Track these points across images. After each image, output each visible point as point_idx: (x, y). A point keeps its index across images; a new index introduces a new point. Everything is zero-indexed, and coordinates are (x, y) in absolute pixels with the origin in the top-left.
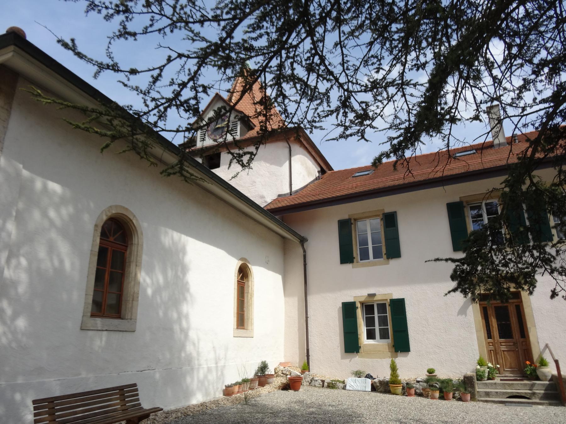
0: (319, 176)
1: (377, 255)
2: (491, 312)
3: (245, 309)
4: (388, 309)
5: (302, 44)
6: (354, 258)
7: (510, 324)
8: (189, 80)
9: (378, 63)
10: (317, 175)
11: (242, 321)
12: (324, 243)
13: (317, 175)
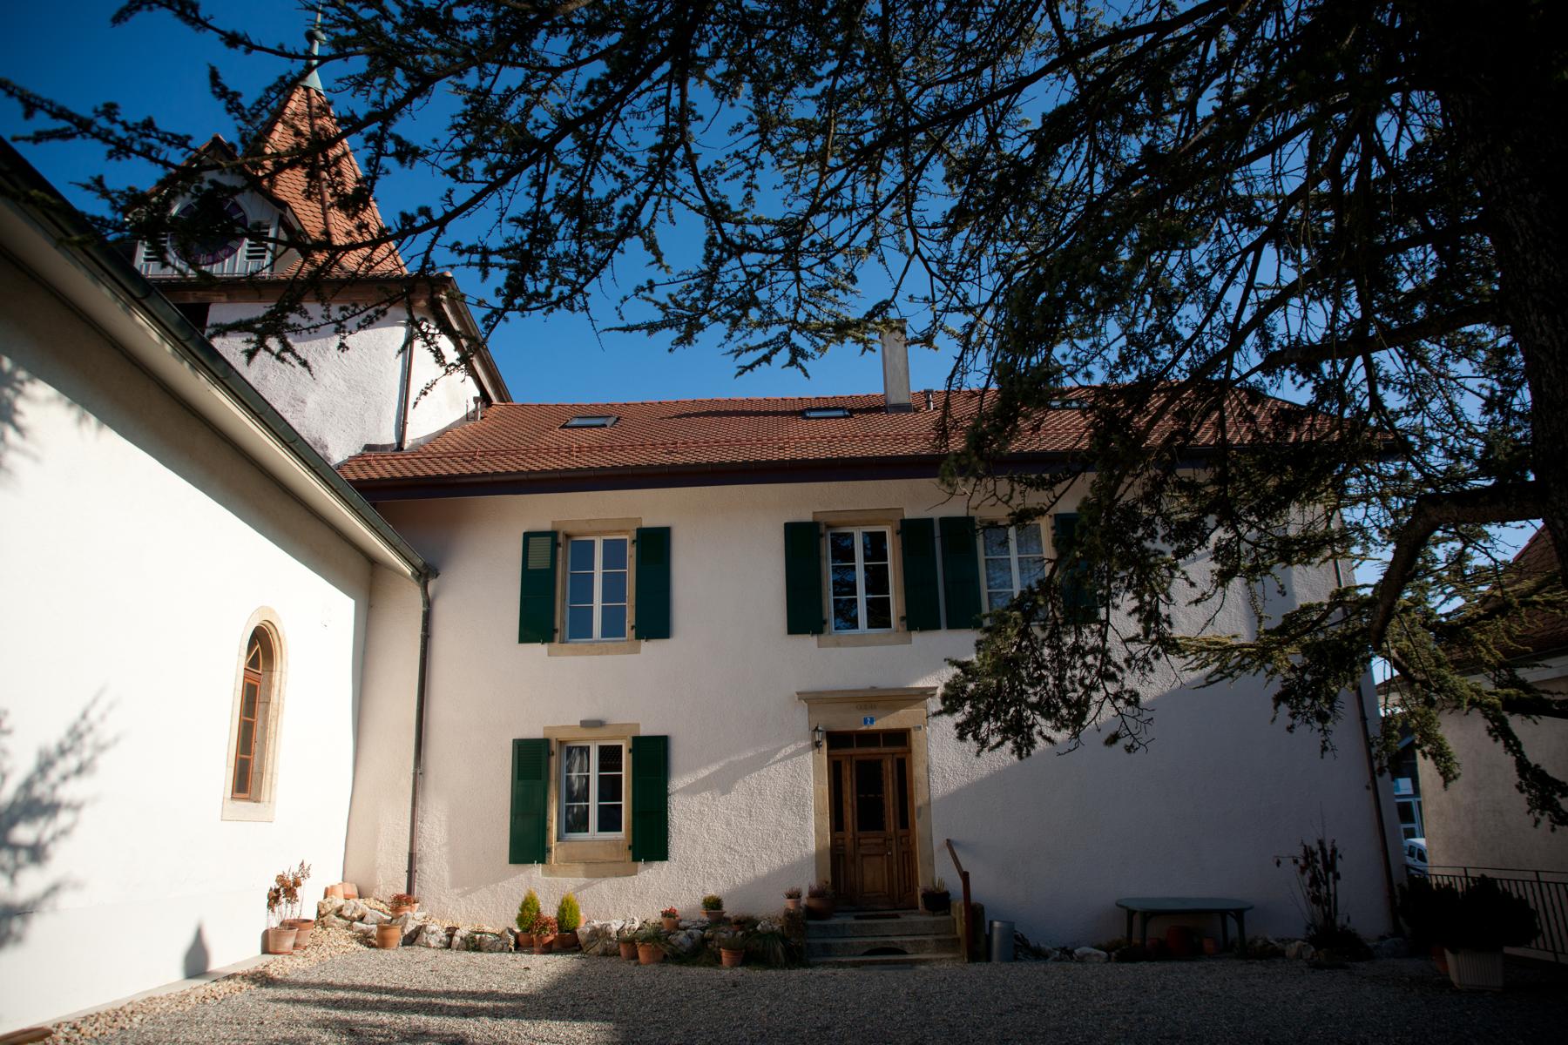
0: (475, 412)
1: (613, 627)
2: (848, 774)
3: (256, 748)
4: (626, 759)
5: (572, 71)
6: (555, 631)
7: (858, 792)
8: (371, 118)
9: (749, 172)
10: (472, 406)
11: (246, 780)
12: (484, 584)
13: (472, 406)
